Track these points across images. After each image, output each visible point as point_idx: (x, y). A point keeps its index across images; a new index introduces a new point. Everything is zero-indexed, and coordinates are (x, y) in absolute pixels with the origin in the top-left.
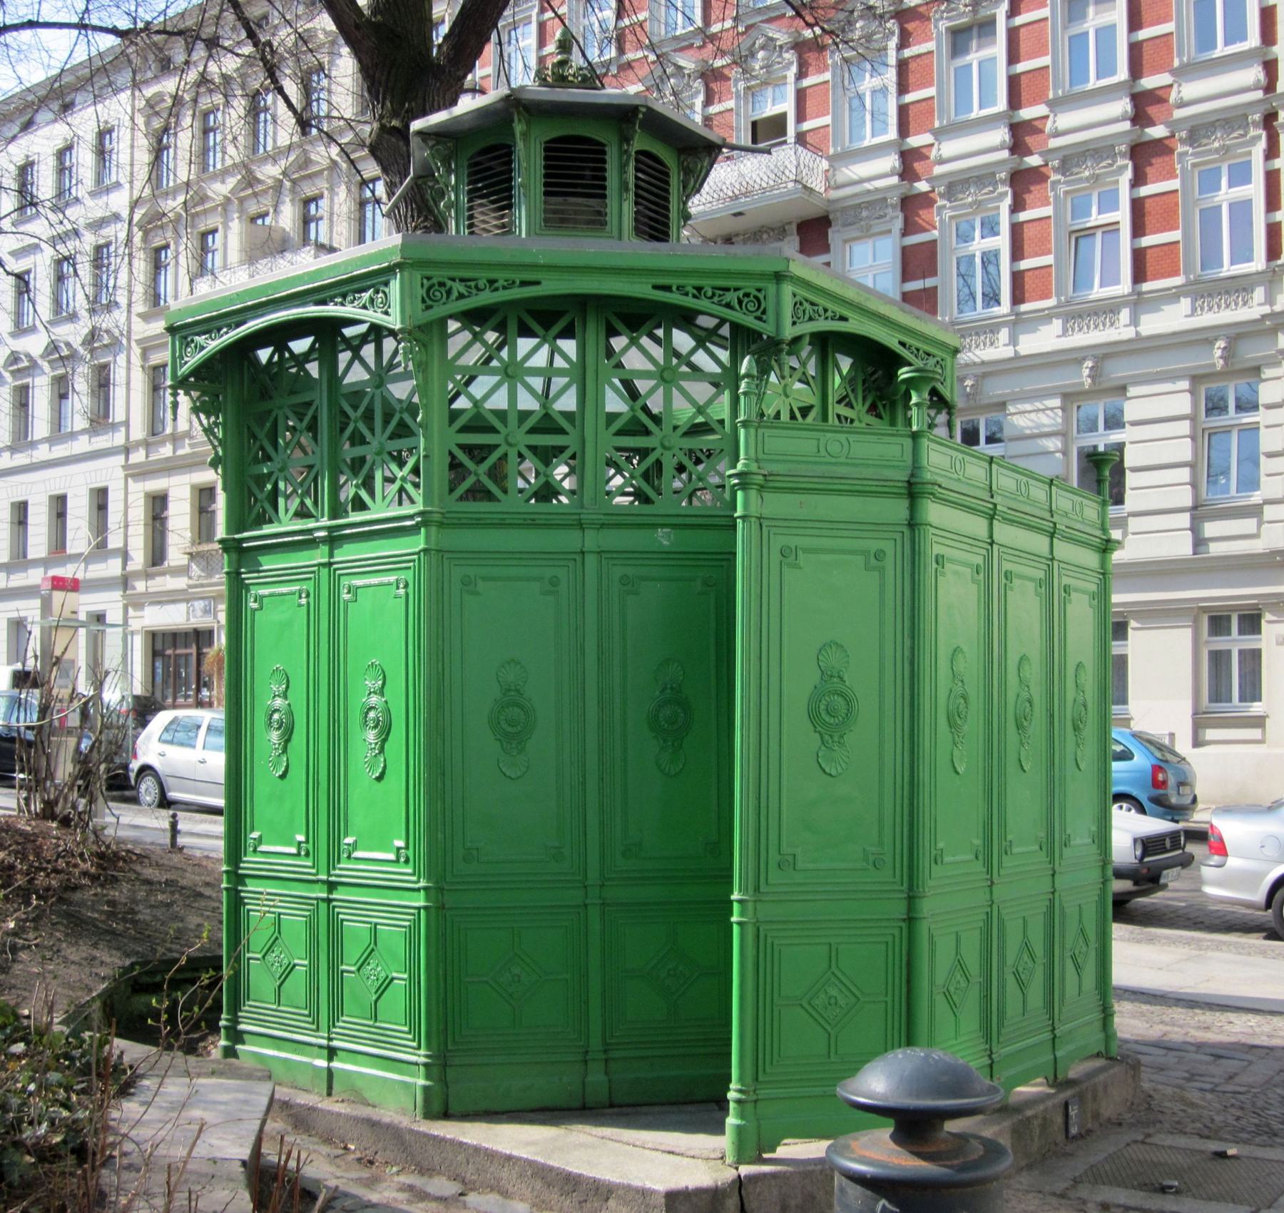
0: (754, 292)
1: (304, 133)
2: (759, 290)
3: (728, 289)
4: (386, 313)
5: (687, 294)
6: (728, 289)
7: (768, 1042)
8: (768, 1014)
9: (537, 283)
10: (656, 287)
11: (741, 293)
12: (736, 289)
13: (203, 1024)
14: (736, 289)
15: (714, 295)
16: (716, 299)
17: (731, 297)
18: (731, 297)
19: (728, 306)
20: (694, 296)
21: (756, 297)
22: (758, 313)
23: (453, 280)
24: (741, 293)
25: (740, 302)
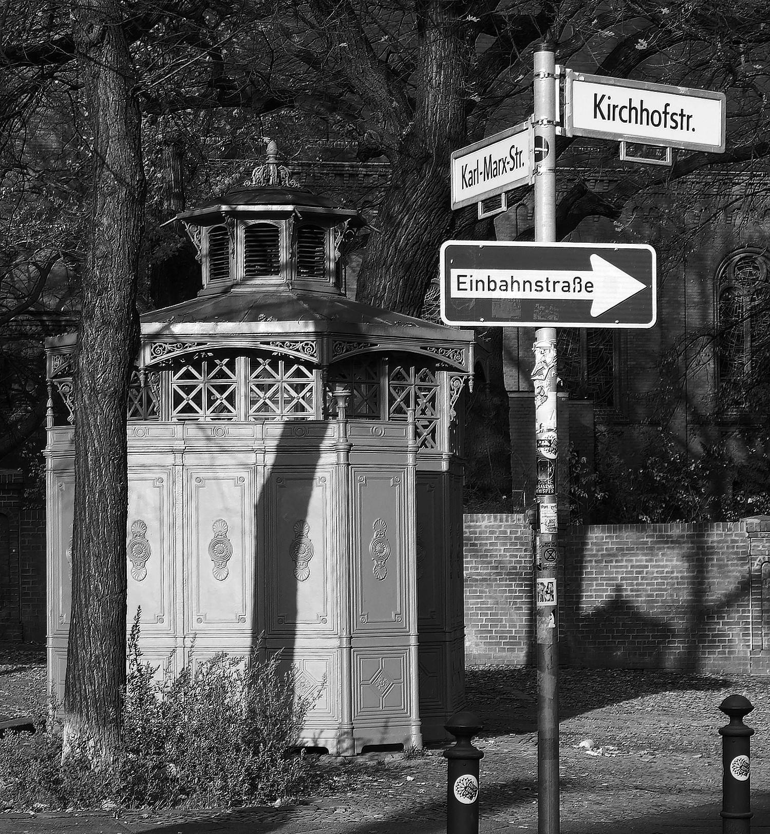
1: (158, 240)
6: (297, 342)
10: (422, 348)
17: (299, 346)
25: (303, 348)
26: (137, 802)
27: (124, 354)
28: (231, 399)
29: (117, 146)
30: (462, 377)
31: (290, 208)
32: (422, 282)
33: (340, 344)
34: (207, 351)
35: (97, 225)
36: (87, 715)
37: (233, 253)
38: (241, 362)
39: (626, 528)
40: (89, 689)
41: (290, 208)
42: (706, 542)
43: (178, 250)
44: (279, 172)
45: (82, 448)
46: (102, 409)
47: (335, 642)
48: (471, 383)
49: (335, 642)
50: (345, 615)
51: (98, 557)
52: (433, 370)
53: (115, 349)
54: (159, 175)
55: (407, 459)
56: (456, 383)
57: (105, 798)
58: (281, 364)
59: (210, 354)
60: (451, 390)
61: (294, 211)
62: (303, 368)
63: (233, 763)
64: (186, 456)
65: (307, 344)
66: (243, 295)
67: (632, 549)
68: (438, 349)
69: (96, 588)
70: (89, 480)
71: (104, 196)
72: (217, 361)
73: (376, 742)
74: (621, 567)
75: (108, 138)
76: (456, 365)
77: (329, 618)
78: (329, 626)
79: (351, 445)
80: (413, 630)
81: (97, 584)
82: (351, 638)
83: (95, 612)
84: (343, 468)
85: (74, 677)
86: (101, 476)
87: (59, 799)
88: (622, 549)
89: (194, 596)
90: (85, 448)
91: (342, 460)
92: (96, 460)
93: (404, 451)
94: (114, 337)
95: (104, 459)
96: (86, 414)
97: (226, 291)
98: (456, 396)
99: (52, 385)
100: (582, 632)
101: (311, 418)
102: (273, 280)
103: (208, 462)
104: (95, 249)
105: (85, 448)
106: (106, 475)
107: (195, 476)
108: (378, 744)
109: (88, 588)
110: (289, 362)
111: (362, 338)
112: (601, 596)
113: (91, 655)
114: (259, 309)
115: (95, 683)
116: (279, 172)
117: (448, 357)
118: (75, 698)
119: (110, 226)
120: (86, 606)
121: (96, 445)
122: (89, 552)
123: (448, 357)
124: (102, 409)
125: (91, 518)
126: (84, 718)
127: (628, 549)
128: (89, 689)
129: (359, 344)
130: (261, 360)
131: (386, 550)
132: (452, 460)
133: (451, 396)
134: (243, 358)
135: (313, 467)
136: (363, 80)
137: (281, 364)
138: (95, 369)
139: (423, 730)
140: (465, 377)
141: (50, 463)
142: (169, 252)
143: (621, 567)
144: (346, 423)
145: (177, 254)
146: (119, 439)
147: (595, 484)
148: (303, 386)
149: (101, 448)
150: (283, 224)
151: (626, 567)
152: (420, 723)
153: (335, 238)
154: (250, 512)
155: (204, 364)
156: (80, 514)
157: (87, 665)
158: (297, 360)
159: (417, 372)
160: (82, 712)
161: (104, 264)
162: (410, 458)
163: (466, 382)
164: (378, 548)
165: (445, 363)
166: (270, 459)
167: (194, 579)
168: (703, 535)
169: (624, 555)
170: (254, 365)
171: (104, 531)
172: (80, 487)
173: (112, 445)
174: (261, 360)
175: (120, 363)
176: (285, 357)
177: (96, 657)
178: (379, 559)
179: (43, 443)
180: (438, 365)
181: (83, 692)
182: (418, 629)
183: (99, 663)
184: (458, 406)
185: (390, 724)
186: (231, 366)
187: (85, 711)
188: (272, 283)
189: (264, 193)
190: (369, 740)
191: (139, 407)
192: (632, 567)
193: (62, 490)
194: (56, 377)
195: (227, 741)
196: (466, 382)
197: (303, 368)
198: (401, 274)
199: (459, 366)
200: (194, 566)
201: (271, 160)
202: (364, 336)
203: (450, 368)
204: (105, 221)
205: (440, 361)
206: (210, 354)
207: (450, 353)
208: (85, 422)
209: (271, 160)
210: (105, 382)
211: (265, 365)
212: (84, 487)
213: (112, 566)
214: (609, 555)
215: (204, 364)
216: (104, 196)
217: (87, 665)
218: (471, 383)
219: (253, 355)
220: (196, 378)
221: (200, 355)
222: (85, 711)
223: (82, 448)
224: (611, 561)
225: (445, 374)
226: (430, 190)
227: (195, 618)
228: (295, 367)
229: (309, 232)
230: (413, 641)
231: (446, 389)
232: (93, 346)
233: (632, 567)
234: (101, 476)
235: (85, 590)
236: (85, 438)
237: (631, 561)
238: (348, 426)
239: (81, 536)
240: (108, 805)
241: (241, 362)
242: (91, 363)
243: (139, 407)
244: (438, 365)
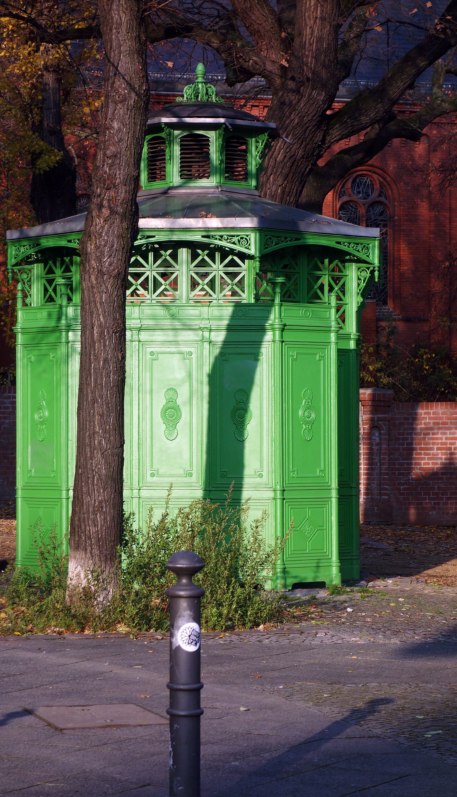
0: (245, 237)
1: (41, 153)
2: (247, 236)
3: (234, 236)
4: (368, 256)
5: (216, 239)
6: (234, 236)
7: (48, 503)
8: (304, 503)
9: (154, 237)
10: (337, 243)
11: (239, 238)
12: (237, 236)
13: (229, 623)
14: (237, 236)
15: (228, 238)
16: (228, 241)
17: (235, 239)
18: (235, 239)
20: (220, 240)
21: (246, 239)
22: (246, 246)
23: (274, 237)
24: (239, 238)
25: (239, 241)
26: (145, 627)
27: (127, 241)
28: (175, 285)
29: (128, 60)
30: (368, 268)
31: (222, 120)
32: (297, 190)
33: (270, 238)
34: (153, 243)
35: (108, 129)
36: (91, 553)
37: (170, 159)
38: (184, 253)
39: (442, 405)
40: (93, 530)
41: (222, 120)
42: (416, 429)
43: (57, 162)
44: (207, 90)
45: (88, 322)
46: (107, 288)
47: (271, 494)
48: (376, 274)
49: (271, 494)
50: (279, 471)
51: (102, 416)
52: (343, 262)
53: (120, 236)
54: (40, 98)
55: (330, 338)
56: (364, 274)
57: (119, 622)
58: (218, 256)
59: (156, 246)
60: (359, 279)
61: (224, 124)
62: (236, 258)
63: (224, 594)
64: (142, 333)
65: (242, 238)
66: (181, 195)
67: (446, 423)
68: (350, 244)
69: (100, 443)
70: (95, 349)
71: (116, 103)
72: (162, 252)
73: (310, 580)
74: (437, 439)
75: (120, 53)
76: (364, 257)
77: (265, 473)
78: (264, 480)
79: (285, 325)
80: (334, 484)
81: (101, 440)
82: (284, 490)
83: (100, 465)
84: (278, 344)
85: (79, 520)
86: (105, 346)
87: (78, 623)
88: (438, 424)
89: (148, 454)
90: (92, 322)
91: (277, 338)
92: (101, 334)
93: (327, 330)
94: (118, 226)
95: (108, 331)
96: (93, 292)
97: (165, 192)
98: (363, 285)
99: (13, 272)
100: (403, 494)
101: (244, 302)
102: (204, 182)
103: (171, 338)
104: (106, 149)
105: (92, 322)
106: (110, 345)
107: (149, 350)
108: (311, 581)
109: (93, 443)
110: (225, 253)
111: (300, 234)
112: (437, 464)
113: (95, 501)
114: (193, 209)
115: (98, 525)
116: (207, 90)
117: (358, 251)
118: (80, 537)
119: (119, 130)
120: (91, 459)
121: (102, 319)
122: (94, 412)
123: (358, 251)
124: (107, 288)
125: (96, 381)
126: (89, 555)
127: (443, 423)
128: (93, 530)
129: (286, 238)
130: (199, 251)
131: (313, 416)
132: (358, 342)
133: (359, 285)
134: (184, 250)
135: (258, 344)
136: (250, 14)
137: (218, 256)
138: (102, 253)
139: (342, 570)
140: (372, 269)
141: (20, 339)
142: (51, 164)
143: (437, 439)
144: (281, 305)
145: (57, 165)
146: (120, 314)
147: (379, 370)
148: (236, 274)
149: (106, 322)
150: (212, 135)
151: (441, 439)
152: (339, 564)
153: (257, 147)
154: (206, 380)
155: (151, 256)
156: (86, 379)
157: (91, 509)
158: (232, 252)
159: (330, 263)
160: (86, 549)
161: (113, 162)
162: (333, 337)
163: (372, 272)
164: (306, 414)
165: (354, 256)
166: (220, 337)
167: (148, 440)
168: (412, 424)
169: (439, 429)
170: (194, 256)
171: (107, 393)
172: (86, 355)
173: (115, 319)
174: (199, 251)
175: (123, 248)
176: (220, 249)
177: (100, 502)
178: (307, 423)
179: (14, 322)
180: (348, 257)
181: (87, 533)
182: (339, 485)
183: (102, 508)
184: (364, 294)
185: (321, 565)
186: (174, 256)
187: (89, 549)
188: (209, 184)
189: (202, 108)
190: (305, 578)
191: (53, 294)
192: (446, 439)
193: (31, 362)
194: (16, 265)
195: (219, 575)
196: (372, 272)
197: (236, 258)
198: (280, 183)
199: (366, 259)
200: (148, 427)
201: (200, 79)
202: (301, 233)
203: (359, 261)
204: (116, 125)
205: (349, 254)
206: (156, 246)
207: (360, 248)
208: (92, 299)
209: (200, 79)
210: (110, 265)
211: (203, 255)
212: (90, 356)
213: (113, 424)
214: (427, 429)
215: (151, 256)
216: (116, 103)
217: (91, 509)
218: (376, 274)
219: (192, 246)
220: (144, 266)
221: (147, 247)
222: (89, 549)
223: (88, 322)
224: (429, 434)
225: (354, 266)
226: (306, 110)
227: (149, 472)
228: (230, 257)
229: (235, 141)
230: (334, 494)
231: (354, 278)
232: (100, 235)
233: (446, 439)
234: (105, 346)
235: (91, 445)
236: (92, 313)
237: (446, 434)
238: (283, 308)
239: (87, 398)
240: (122, 629)
241: (184, 253)
242: (99, 248)
243: (53, 294)
244: (348, 257)
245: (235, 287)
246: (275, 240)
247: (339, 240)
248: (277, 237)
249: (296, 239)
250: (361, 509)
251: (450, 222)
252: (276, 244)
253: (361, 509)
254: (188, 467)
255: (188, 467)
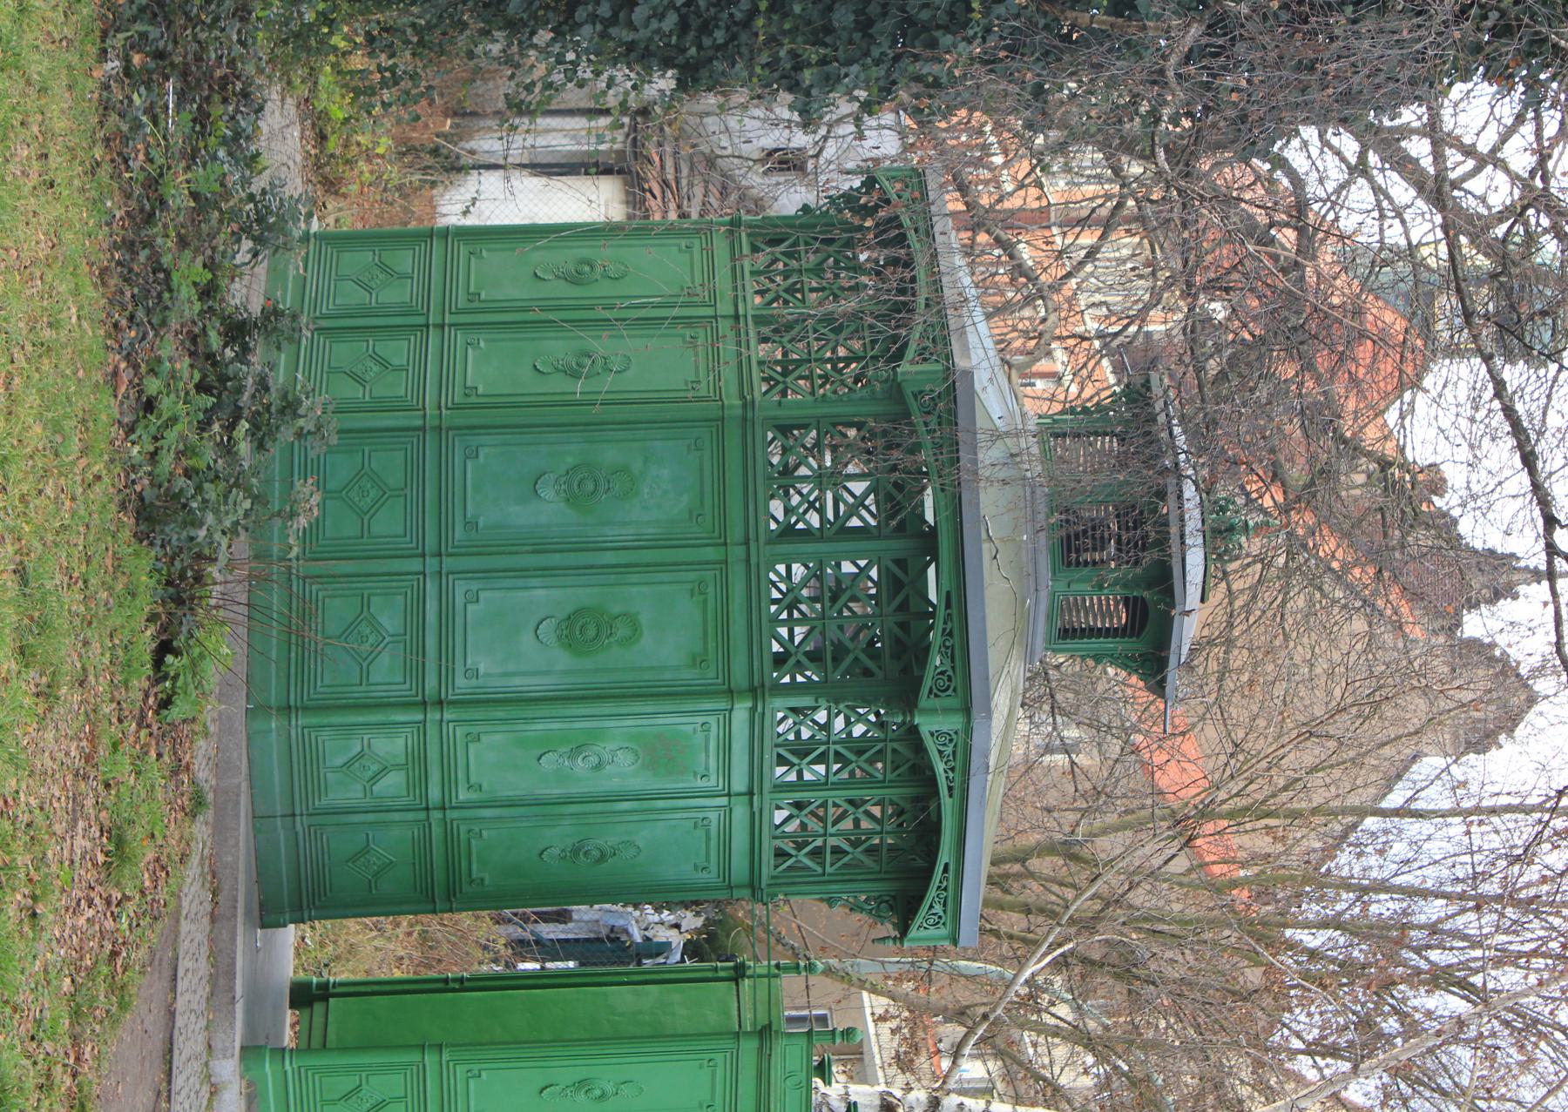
3: (953, 660)
6: (953, 660)
10: (946, 865)
11: (950, 673)
19: (931, 907)
24: (950, 673)
65: (950, 679)
129: (952, 769)
245: (851, 657)
246: (949, 750)
247: (951, 868)
248: (954, 753)
249: (950, 789)
250: (277, 790)
251: (164, 648)
252: (940, 752)
253: (277, 790)
254: (701, 860)
255: (701, 860)
